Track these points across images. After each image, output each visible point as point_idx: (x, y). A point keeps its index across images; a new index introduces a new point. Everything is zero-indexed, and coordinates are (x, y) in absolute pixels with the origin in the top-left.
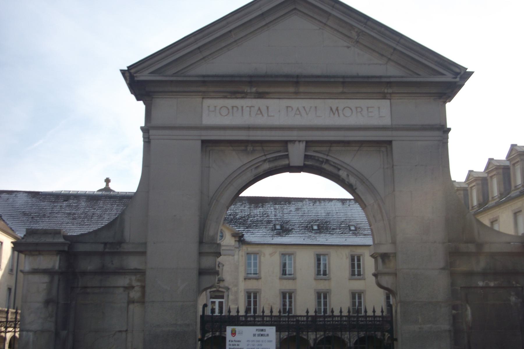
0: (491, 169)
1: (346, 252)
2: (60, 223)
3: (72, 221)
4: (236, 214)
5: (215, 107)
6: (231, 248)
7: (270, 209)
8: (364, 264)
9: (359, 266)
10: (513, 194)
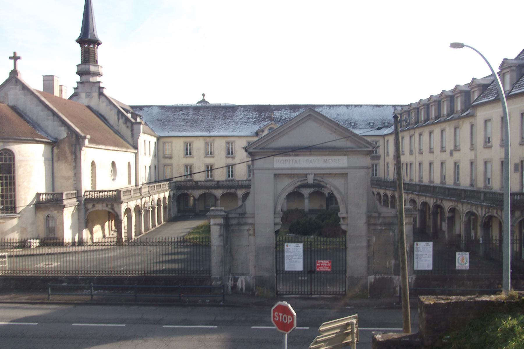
10: (442, 119)
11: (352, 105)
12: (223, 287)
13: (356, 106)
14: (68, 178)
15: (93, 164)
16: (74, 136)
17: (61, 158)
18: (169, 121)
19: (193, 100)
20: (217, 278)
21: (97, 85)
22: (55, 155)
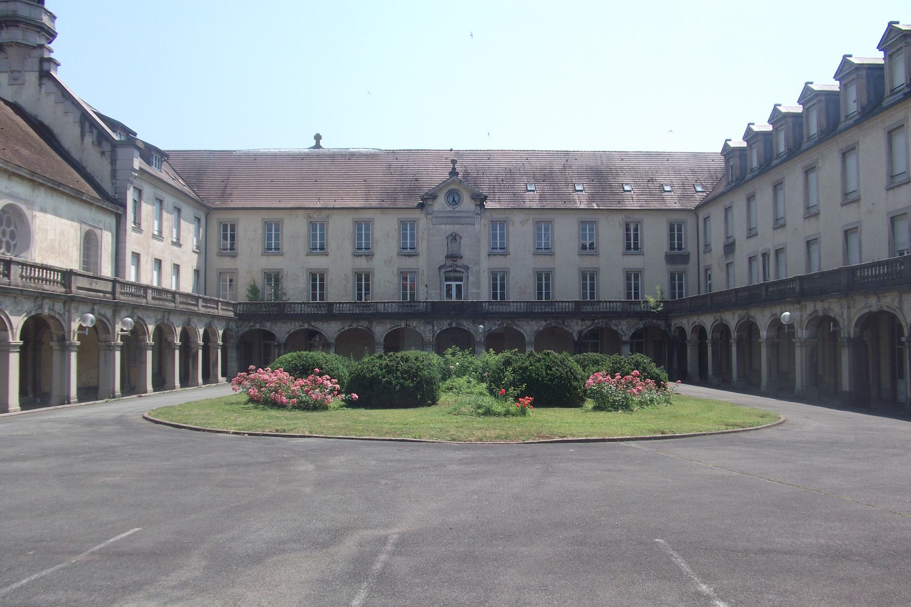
21: (36, 53)
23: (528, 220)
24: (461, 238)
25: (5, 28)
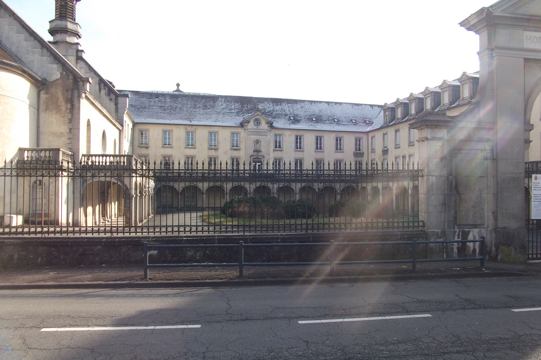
0: (444, 87)
1: (333, 136)
2: (156, 112)
3: (164, 111)
4: (265, 109)
5: (530, 37)
6: (265, 131)
7: (285, 107)
8: (323, 142)
9: (321, 144)
11: (332, 102)
12: (445, 247)
13: (336, 103)
14: (61, 135)
15: (89, 121)
16: (71, 77)
17: (50, 107)
18: (145, 107)
19: (170, 89)
20: (438, 233)
21: (74, 47)
22: (42, 102)
23: (292, 134)
24: (261, 142)
25: (59, 34)
